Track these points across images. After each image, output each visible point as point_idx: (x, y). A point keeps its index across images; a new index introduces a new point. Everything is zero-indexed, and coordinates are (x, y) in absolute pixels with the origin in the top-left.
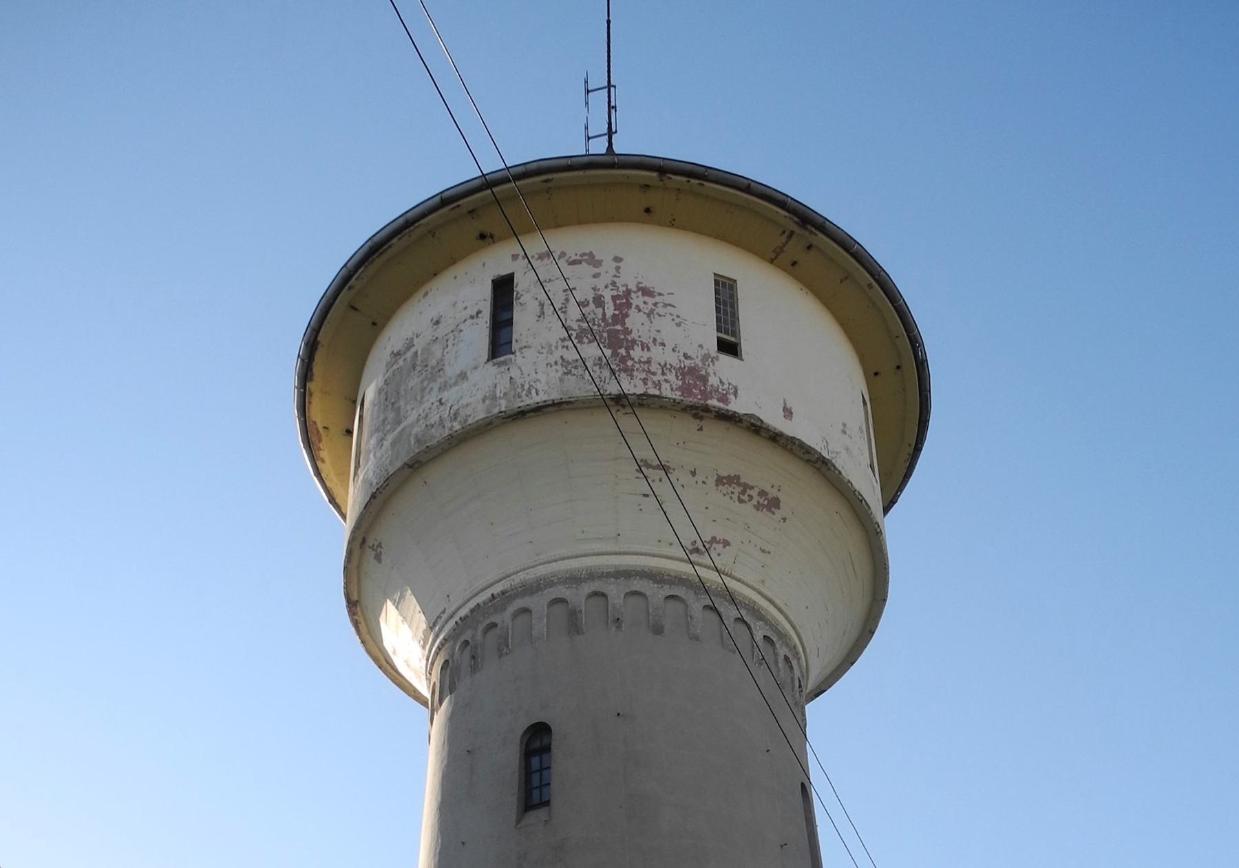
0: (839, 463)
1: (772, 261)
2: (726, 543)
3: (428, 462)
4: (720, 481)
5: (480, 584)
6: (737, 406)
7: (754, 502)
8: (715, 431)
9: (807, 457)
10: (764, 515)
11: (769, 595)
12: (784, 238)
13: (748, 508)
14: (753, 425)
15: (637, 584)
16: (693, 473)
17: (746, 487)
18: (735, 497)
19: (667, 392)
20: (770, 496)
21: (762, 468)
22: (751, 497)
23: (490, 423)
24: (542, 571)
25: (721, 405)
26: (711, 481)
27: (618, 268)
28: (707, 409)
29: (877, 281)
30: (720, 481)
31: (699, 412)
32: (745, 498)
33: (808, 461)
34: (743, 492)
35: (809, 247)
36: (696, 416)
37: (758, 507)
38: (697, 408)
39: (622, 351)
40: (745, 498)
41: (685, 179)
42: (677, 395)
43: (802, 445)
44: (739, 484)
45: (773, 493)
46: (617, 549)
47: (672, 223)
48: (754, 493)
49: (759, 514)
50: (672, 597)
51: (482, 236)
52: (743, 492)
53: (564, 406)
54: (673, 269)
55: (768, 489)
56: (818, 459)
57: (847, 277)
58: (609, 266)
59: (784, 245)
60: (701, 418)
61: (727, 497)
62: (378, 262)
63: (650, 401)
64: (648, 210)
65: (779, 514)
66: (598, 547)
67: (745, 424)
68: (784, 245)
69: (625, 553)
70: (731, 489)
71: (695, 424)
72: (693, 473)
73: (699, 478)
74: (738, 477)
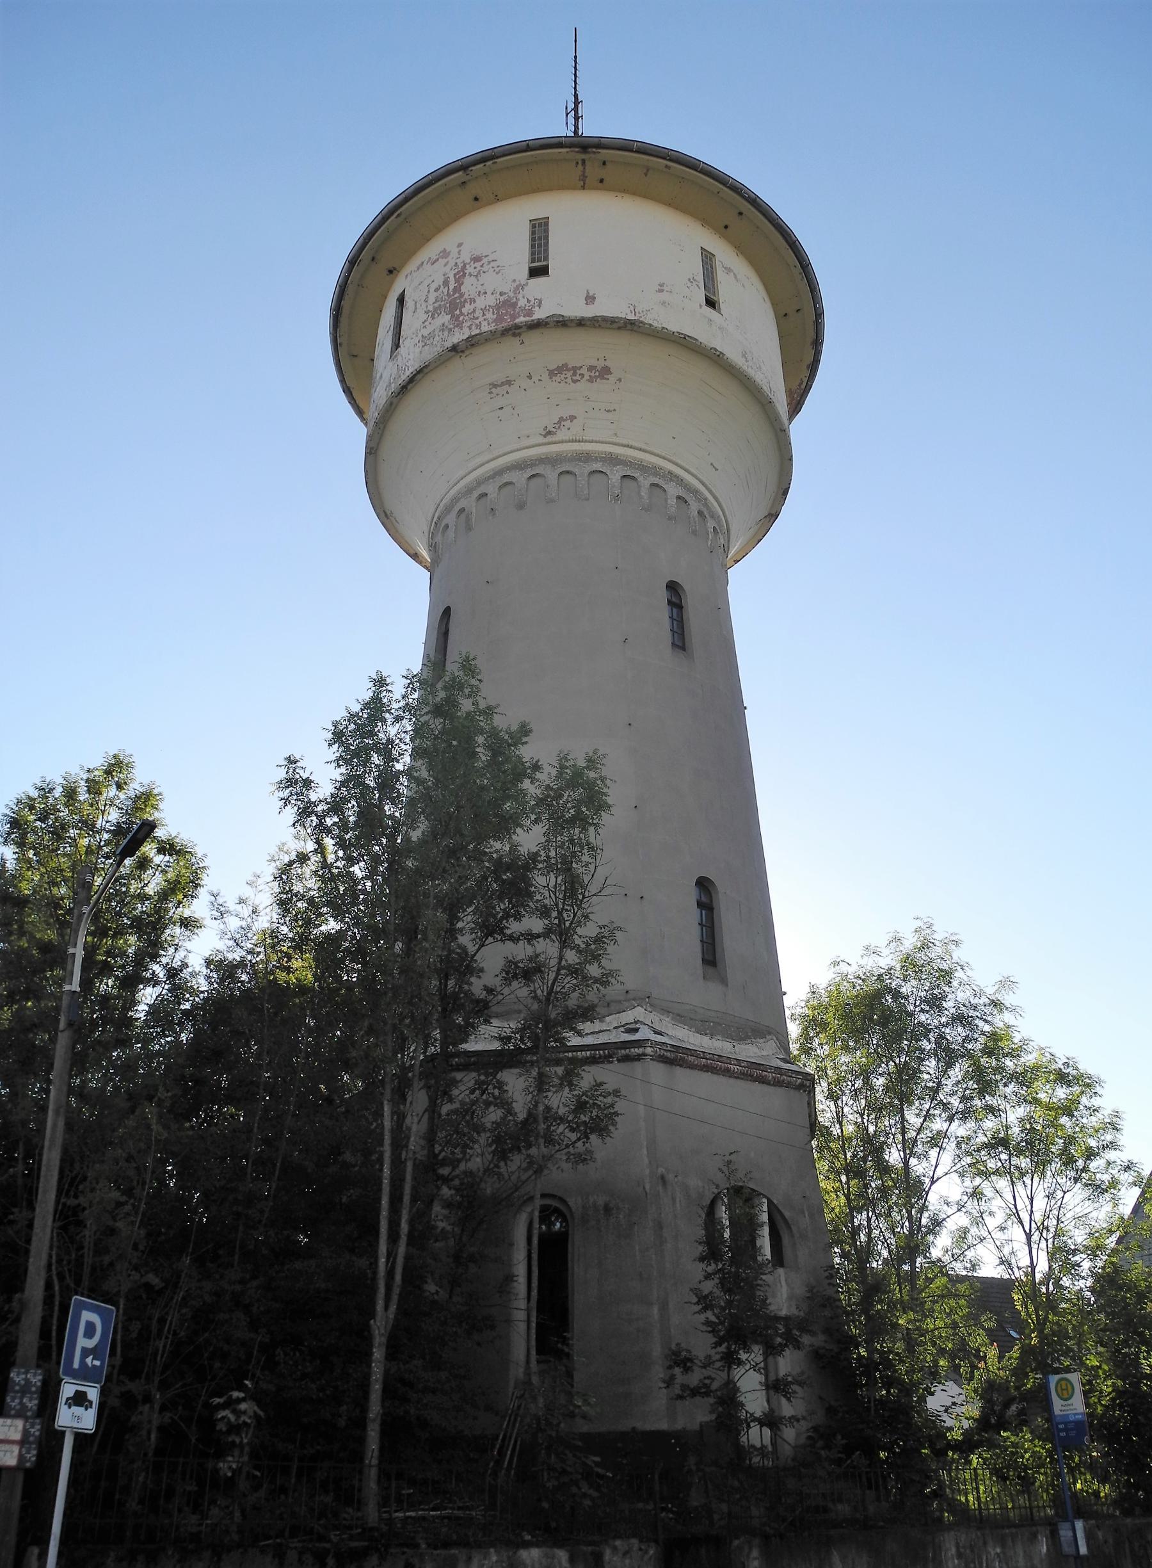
0: (648, 319)
1: (583, 188)
2: (572, 418)
3: (378, 444)
4: (552, 374)
5: (430, 515)
6: (540, 314)
7: (587, 377)
8: (533, 339)
9: (615, 325)
10: (600, 384)
11: (625, 442)
12: (580, 167)
13: (583, 385)
14: (558, 322)
15: (506, 478)
16: (530, 377)
17: (575, 370)
18: (569, 380)
19: (485, 328)
20: (599, 368)
21: (583, 350)
22: (582, 375)
23: (391, 404)
24: (453, 492)
25: (527, 319)
26: (545, 376)
27: (459, 252)
28: (517, 327)
29: (670, 160)
30: (552, 374)
31: (514, 331)
32: (578, 377)
33: (619, 328)
34: (575, 374)
35: (604, 163)
36: (514, 335)
37: (591, 380)
38: (510, 329)
39: (457, 312)
40: (578, 377)
41: (481, 165)
42: (492, 327)
43: (605, 319)
44: (568, 370)
45: (600, 364)
46: (491, 457)
47: (497, 199)
48: (584, 371)
49: (595, 385)
50: (534, 476)
51: (391, 272)
52: (575, 374)
53: (426, 370)
54: (492, 237)
55: (594, 363)
56: (625, 323)
57: (647, 170)
58: (454, 254)
59: (584, 172)
60: (519, 335)
61: (563, 383)
62: (344, 320)
63: (476, 339)
64: (602, 181)
65: (612, 378)
66: (479, 461)
67: (552, 324)
68: (584, 172)
69: (511, 452)
70: (563, 376)
71: (517, 341)
72: (530, 377)
73: (535, 378)
74: (565, 365)
